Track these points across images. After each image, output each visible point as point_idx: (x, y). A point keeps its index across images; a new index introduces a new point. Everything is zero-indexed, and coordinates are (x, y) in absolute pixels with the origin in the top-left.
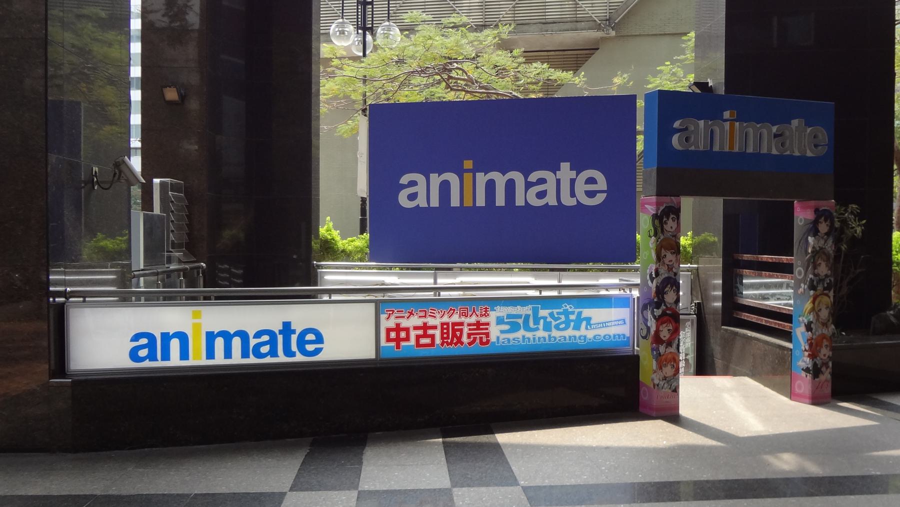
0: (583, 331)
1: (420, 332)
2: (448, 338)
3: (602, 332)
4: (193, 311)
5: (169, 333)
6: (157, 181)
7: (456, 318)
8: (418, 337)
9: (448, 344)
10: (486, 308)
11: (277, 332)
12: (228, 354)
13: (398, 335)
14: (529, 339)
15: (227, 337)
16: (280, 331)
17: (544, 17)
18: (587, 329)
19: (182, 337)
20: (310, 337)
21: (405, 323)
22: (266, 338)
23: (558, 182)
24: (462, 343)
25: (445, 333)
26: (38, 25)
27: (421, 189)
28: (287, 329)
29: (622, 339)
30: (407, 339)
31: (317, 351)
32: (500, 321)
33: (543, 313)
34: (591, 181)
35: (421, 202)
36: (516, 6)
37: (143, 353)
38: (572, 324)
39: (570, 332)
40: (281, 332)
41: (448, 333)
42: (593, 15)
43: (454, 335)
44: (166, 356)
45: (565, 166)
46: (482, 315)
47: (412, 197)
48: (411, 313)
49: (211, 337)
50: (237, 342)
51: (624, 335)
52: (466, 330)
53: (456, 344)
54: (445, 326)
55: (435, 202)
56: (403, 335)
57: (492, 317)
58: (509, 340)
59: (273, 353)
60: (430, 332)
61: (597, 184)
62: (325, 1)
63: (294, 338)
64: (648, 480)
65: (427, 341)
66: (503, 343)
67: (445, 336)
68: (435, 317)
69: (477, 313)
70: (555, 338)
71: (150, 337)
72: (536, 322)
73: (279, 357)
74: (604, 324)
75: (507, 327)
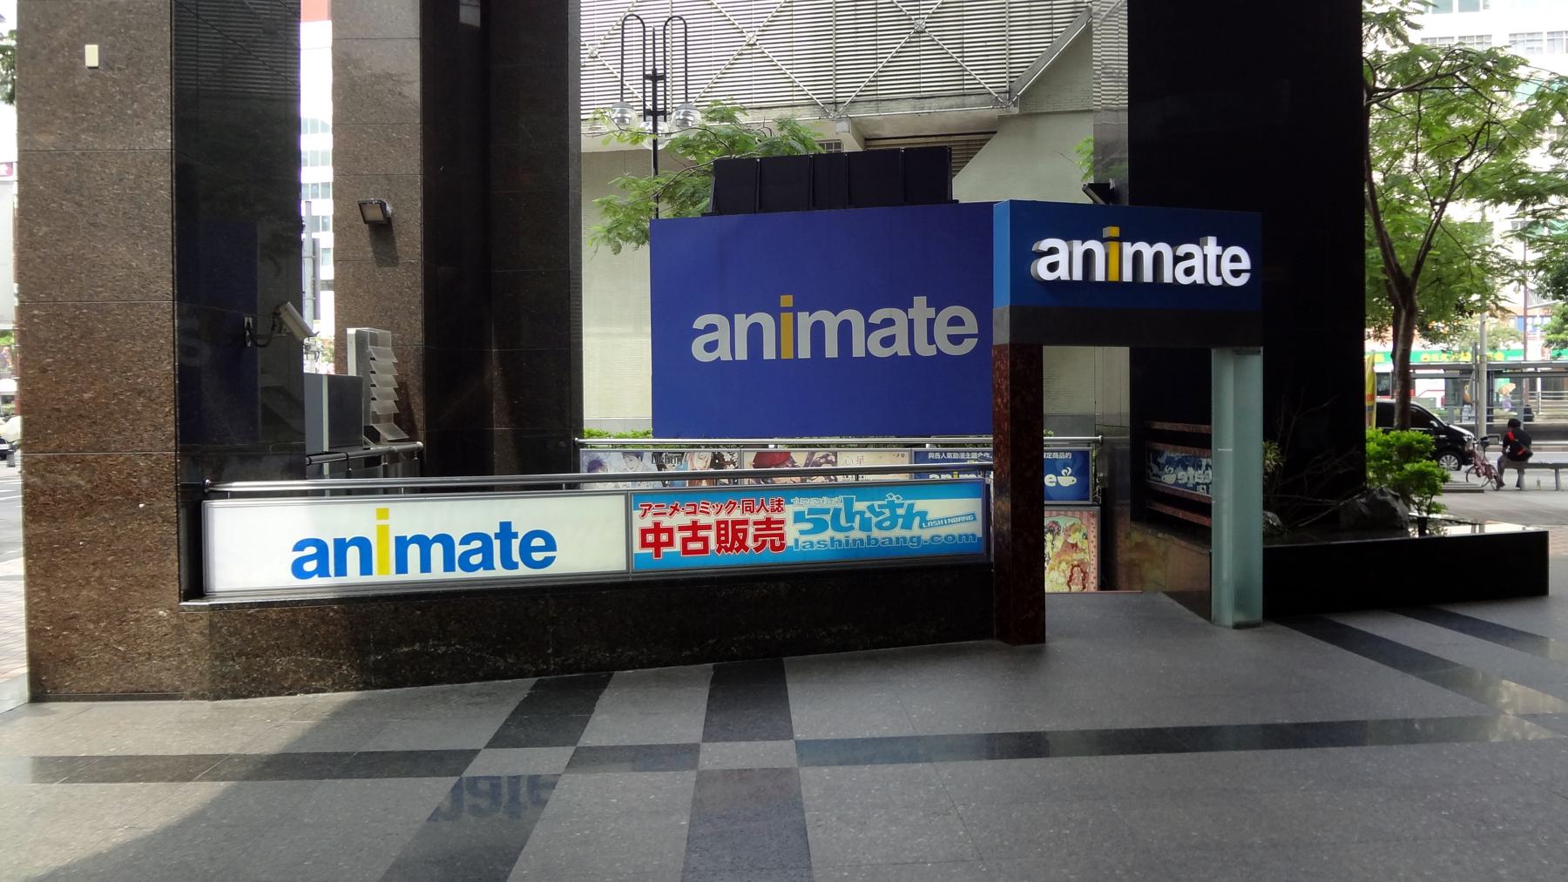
0: (916, 531)
1: (688, 534)
2: (726, 541)
3: (943, 531)
4: (378, 509)
5: (345, 539)
6: (351, 331)
7: (737, 514)
8: (685, 541)
9: (727, 550)
10: (779, 501)
11: (493, 537)
12: (426, 566)
13: (657, 538)
14: (840, 541)
15: (424, 542)
16: (496, 534)
17: (918, 90)
18: (921, 527)
19: (363, 544)
20: (538, 542)
21: (666, 522)
22: (477, 544)
23: (911, 322)
24: (746, 549)
25: (723, 535)
26: (161, 133)
27: (722, 335)
28: (506, 531)
29: (971, 540)
30: (670, 543)
31: (548, 561)
32: (799, 517)
33: (860, 506)
34: (1235, 259)
35: (723, 353)
36: (879, 74)
37: (310, 566)
38: (900, 521)
39: (898, 532)
40: (497, 536)
41: (726, 535)
42: (987, 86)
43: (735, 537)
44: (341, 570)
45: (920, 301)
46: (773, 510)
47: (1053, 267)
48: (675, 509)
49: (402, 543)
50: (437, 551)
51: (973, 535)
52: (751, 530)
53: (738, 550)
54: (723, 526)
55: (742, 354)
56: (664, 537)
57: (788, 513)
58: (812, 544)
59: (487, 563)
60: (702, 533)
61: (964, 325)
62: (892, 3)
63: (516, 544)
64: (969, 731)
65: (698, 546)
66: (804, 547)
67: (723, 538)
68: (708, 513)
69: (767, 507)
70: (877, 540)
71: (320, 544)
72: (850, 518)
73: (494, 569)
74: (945, 521)
75: (808, 526)
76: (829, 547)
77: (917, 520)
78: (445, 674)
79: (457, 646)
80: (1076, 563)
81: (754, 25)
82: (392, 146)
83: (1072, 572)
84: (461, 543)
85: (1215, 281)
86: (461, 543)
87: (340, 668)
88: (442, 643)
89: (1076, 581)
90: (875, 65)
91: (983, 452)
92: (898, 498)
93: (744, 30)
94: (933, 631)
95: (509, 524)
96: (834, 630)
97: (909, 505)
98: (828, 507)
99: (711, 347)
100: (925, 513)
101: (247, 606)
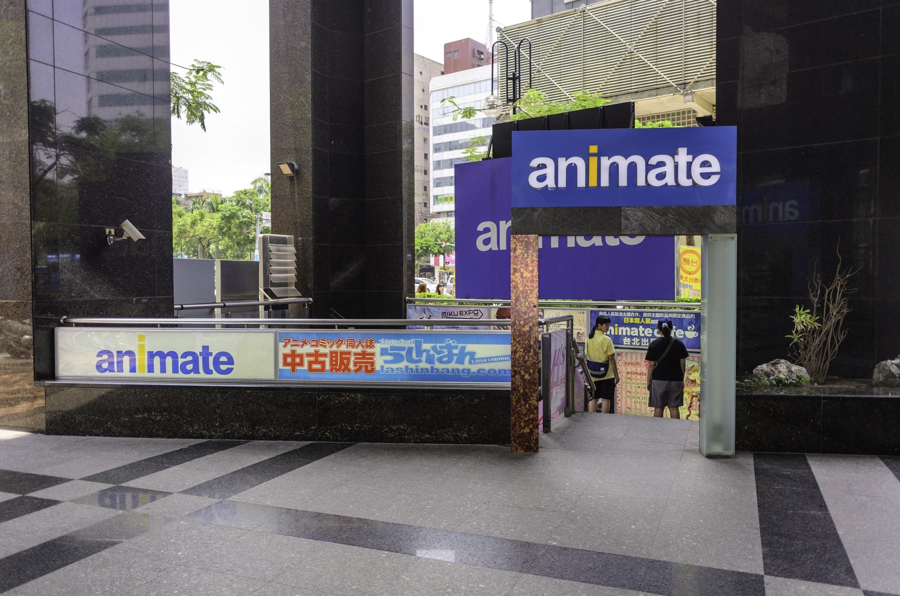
0: (466, 365)
1: (312, 359)
2: (336, 365)
7: (343, 348)
8: (310, 363)
9: (337, 370)
10: (371, 340)
12: (163, 370)
14: (412, 369)
18: (470, 362)
19: (130, 353)
20: (223, 359)
21: (299, 350)
22: (190, 358)
24: (349, 370)
25: (334, 361)
30: (301, 364)
31: (229, 371)
32: (384, 352)
33: (426, 346)
34: (705, 164)
38: (455, 358)
41: (336, 361)
43: (342, 363)
44: (121, 370)
46: (367, 347)
47: (542, 178)
49: (151, 355)
52: (353, 358)
54: (334, 355)
57: (377, 348)
59: (197, 370)
63: (211, 359)
65: (318, 366)
66: (387, 371)
70: (438, 370)
74: (489, 360)
75: (390, 358)
76: (404, 372)
77: (467, 359)
78: (161, 432)
79: (167, 416)
80: (694, 394)
81: (633, 40)
82: (298, 131)
83: (691, 400)
84: (181, 357)
85: (685, 182)
86: (182, 357)
87: (107, 423)
88: (159, 414)
89: (694, 407)
90: (711, 56)
91: (635, 312)
92: (454, 342)
93: (627, 44)
94: (465, 435)
95: (208, 347)
96: (394, 428)
97: (462, 347)
98: (404, 346)
99: (542, 178)
100: (474, 353)
101: (62, 386)
